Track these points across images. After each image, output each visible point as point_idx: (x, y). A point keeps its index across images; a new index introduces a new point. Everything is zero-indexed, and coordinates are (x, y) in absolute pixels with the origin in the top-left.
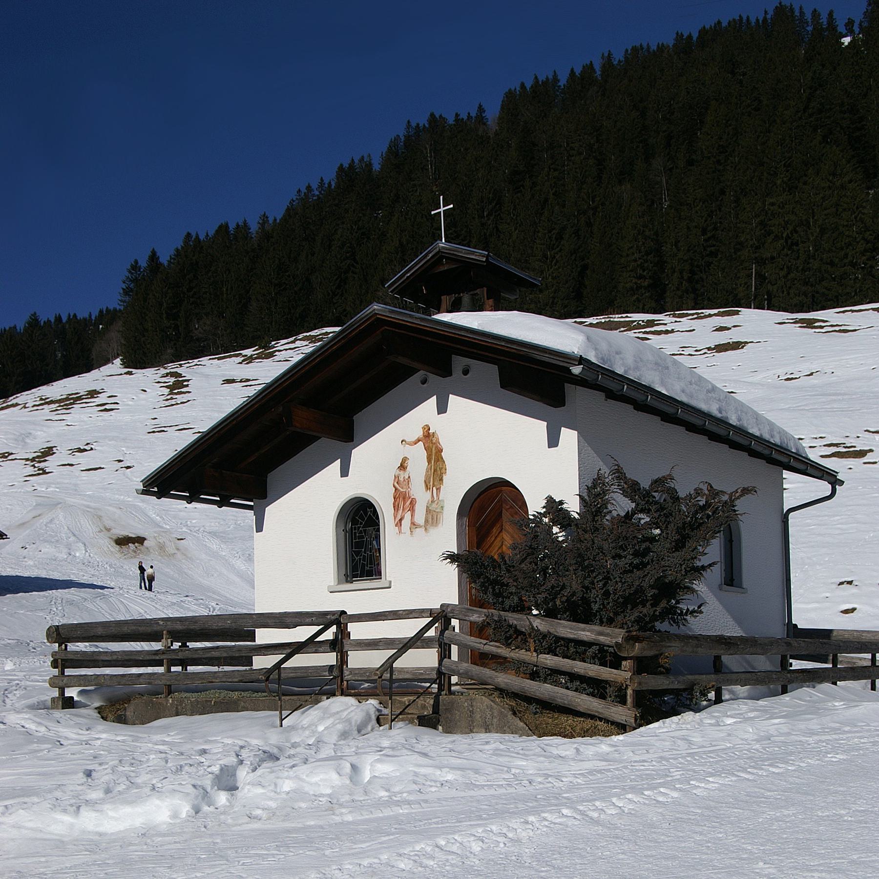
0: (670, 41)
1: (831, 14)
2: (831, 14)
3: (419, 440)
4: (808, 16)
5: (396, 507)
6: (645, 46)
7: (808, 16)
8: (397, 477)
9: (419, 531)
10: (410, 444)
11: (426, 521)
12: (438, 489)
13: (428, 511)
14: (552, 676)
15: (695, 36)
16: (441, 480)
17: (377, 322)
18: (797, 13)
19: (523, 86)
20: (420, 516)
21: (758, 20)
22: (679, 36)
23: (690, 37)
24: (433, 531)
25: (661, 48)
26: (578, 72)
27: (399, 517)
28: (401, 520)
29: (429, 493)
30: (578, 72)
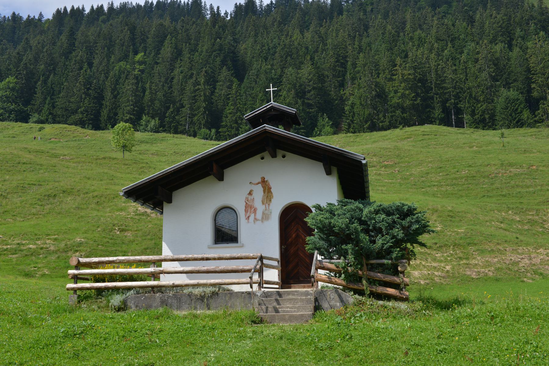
0: (142, 4)
1: (218, 8)
2: (218, 8)
3: (259, 183)
4: (208, 7)
5: (246, 211)
6: (130, 2)
7: (208, 7)
8: (247, 199)
9: (259, 223)
10: (254, 184)
11: (263, 218)
12: (269, 205)
13: (263, 213)
14: (131, 277)
15: (155, 3)
16: (270, 201)
17: (265, 132)
18: (203, 4)
19: (65, 9)
20: (259, 215)
21: (184, 2)
22: (147, 3)
23: (152, 3)
24: (266, 223)
25: (138, 6)
26: (95, 7)
27: (248, 215)
28: (249, 217)
29: (264, 206)
30: (95, 7)
